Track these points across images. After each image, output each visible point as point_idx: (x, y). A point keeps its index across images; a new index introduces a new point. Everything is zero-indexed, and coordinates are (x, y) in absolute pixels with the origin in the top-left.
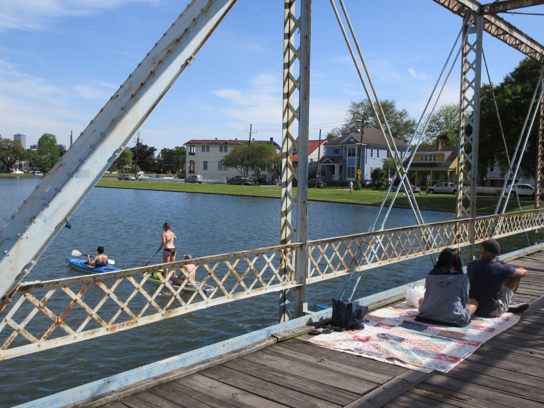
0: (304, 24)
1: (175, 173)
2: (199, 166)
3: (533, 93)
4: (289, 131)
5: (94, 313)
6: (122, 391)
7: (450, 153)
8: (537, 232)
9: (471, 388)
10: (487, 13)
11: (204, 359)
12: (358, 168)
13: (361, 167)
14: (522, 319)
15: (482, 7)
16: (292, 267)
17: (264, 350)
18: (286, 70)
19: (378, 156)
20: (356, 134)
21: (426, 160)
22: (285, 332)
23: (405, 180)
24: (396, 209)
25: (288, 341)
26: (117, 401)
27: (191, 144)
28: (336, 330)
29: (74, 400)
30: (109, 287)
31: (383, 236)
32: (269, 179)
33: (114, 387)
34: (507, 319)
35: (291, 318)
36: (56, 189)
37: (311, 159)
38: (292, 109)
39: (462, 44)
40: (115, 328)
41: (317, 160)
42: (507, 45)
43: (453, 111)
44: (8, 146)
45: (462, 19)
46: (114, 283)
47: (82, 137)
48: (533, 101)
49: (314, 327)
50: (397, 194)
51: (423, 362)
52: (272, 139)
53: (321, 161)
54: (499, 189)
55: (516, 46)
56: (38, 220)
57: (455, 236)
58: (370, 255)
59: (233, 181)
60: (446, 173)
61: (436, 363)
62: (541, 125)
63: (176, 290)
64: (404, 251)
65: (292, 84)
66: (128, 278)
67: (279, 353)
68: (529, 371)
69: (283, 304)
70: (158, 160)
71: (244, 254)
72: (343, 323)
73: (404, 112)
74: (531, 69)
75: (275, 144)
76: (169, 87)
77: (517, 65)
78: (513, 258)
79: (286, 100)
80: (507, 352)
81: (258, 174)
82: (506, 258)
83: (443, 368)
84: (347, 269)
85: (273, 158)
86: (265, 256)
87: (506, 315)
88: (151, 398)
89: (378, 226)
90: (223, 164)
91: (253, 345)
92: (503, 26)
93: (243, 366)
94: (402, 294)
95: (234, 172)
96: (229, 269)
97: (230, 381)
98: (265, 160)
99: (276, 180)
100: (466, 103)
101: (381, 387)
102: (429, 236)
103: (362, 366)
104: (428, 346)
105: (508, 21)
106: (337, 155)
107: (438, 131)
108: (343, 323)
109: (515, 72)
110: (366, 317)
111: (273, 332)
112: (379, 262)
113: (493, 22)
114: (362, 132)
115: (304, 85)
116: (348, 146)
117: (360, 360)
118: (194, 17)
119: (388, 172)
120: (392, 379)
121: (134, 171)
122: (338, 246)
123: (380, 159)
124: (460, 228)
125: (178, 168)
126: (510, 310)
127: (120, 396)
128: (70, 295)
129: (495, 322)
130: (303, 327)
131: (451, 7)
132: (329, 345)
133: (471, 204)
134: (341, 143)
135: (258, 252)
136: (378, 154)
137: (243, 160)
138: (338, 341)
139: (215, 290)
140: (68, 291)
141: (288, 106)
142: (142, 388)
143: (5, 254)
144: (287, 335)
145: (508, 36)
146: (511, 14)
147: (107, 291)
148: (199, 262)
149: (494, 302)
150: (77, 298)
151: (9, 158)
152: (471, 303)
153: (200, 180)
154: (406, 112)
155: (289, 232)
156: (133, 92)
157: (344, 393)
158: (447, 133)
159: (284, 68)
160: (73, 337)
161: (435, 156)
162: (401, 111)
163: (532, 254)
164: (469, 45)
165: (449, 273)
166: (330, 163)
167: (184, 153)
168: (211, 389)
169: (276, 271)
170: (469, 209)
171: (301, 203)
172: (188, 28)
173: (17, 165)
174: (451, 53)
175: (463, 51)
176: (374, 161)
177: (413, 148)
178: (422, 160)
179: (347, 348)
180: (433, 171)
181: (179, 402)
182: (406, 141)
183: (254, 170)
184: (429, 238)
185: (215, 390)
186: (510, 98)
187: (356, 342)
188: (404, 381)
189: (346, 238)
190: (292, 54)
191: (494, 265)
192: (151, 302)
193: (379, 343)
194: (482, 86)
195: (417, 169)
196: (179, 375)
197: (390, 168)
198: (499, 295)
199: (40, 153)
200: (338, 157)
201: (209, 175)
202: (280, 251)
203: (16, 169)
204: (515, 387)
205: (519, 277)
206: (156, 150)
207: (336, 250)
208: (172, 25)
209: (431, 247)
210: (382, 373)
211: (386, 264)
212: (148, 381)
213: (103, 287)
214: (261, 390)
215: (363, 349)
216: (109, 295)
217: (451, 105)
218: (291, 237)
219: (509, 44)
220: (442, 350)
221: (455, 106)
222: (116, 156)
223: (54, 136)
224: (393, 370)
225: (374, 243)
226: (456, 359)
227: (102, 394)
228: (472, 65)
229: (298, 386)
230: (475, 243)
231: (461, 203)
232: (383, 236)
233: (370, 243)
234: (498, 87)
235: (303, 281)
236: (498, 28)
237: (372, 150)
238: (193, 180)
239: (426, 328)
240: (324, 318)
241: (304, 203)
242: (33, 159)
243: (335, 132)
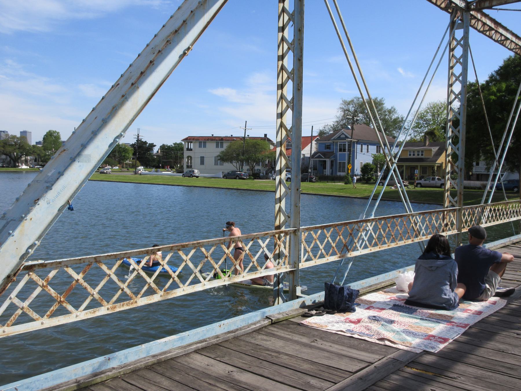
0: (297, 17)
1: (173, 168)
2: (196, 161)
5: (95, 292)
7: (437, 148)
9: (460, 368)
10: (473, 10)
11: (201, 339)
12: (349, 163)
13: (351, 162)
14: (508, 303)
16: (286, 252)
17: (259, 331)
18: (280, 63)
19: (368, 152)
20: (346, 131)
21: (414, 155)
22: (279, 314)
24: (383, 202)
26: (117, 377)
27: (189, 140)
28: (328, 313)
29: (75, 376)
30: (110, 268)
31: (374, 223)
32: (263, 173)
33: (114, 364)
34: (494, 303)
35: (285, 301)
36: (59, 173)
37: (304, 155)
38: (286, 100)
39: (450, 39)
40: (115, 307)
41: (309, 156)
42: (493, 41)
43: (440, 108)
44: (15, 142)
45: (449, 15)
46: (114, 264)
47: (84, 123)
49: (307, 310)
50: (385, 188)
51: (413, 342)
52: (266, 135)
53: (313, 156)
54: (485, 182)
55: (501, 42)
56: (41, 202)
57: (443, 225)
58: (361, 241)
59: (227, 176)
60: (433, 167)
61: (425, 344)
63: (174, 272)
64: (393, 238)
65: (285, 76)
67: (274, 334)
69: (277, 288)
72: (335, 306)
73: (392, 110)
74: (515, 67)
75: (269, 140)
76: (167, 76)
77: (501, 63)
78: (499, 246)
79: (280, 91)
81: (252, 169)
82: (490, 246)
83: (433, 348)
84: (339, 255)
86: (260, 241)
89: (369, 214)
90: (220, 159)
92: (489, 23)
93: (239, 346)
94: (392, 280)
95: (229, 167)
96: (225, 253)
97: (226, 359)
98: (259, 156)
99: (270, 174)
100: (453, 96)
102: (418, 225)
103: (354, 346)
104: (418, 327)
105: (493, 17)
106: (328, 150)
107: (425, 127)
108: (335, 306)
109: (499, 70)
110: (357, 301)
111: (267, 314)
112: (369, 249)
113: (479, 18)
114: (353, 128)
115: (297, 76)
116: (339, 142)
117: (352, 341)
118: (192, 9)
119: (377, 167)
120: (383, 358)
121: (134, 166)
122: (330, 232)
123: (369, 154)
124: (448, 217)
125: (176, 163)
126: (497, 295)
127: (120, 372)
129: (482, 306)
130: (297, 309)
131: (438, 3)
132: (322, 326)
133: (458, 194)
135: (253, 237)
137: (238, 155)
138: (331, 322)
139: (211, 275)
140: (71, 271)
141: (282, 97)
142: (141, 365)
143: (10, 234)
144: (281, 316)
145: (493, 32)
146: (496, 11)
147: (108, 272)
149: (481, 286)
150: (79, 278)
151: (15, 154)
152: (459, 287)
153: (197, 175)
154: (395, 110)
155: (283, 218)
157: (336, 371)
158: (434, 129)
159: (278, 60)
160: (75, 316)
161: (422, 152)
162: (390, 108)
163: (517, 243)
164: (456, 40)
165: (438, 258)
166: (322, 158)
167: (182, 149)
168: (208, 367)
170: (456, 199)
171: (295, 195)
173: (23, 161)
176: (364, 157)
177: (399, 145)
178: (410, 155)
179: (339, 330)
180: (421, 166)
181: (177, 378)
182: (394, 137)
183: (248, 165)
184: (418, 226)
185: (211, 368)
186: (495, 95)
187: (348, 324)
188: (395, 360)
189: (338, 225)
190: (286, 47)
193: (370, 325)
195: (405, 164)
196: (177, 354)
197: (379, 163)
198: (486, 280)
199: (45, 148)
202: (274, 236)
203: (22, 164)
204: (503, 367)
205: (506, 262)
206: (155, 146)
207: (328, 236)
208: (171, 17)
209: (420, 234)
210: (373, 352)
211: (376, 250)
212: (147, 359)
213: (104, 267)
214: (256, 368)
215: (355, 330)
216: (109, 275)
217: (438, 103)
218: (285, 222)
219: (494, 40)
220: (431, 331)
221: (441, 103)
223: (58, 133)
224: (384, 350)
225: (364, 230)
226: (445, 340)
227: (103, 371)
228: (459, 59)
230: (462, 232)
231: (449, 193)
232: (374, 223)
233: (361, 230)
234: (483, 85)
235: (296, 265)
236: (484, 24)
237: (362, 145)
238: (191, 175)
239: (415, 311)
240: (317, 301)
241: (298, 190)
242: (39, 155)
243: (327, 129)
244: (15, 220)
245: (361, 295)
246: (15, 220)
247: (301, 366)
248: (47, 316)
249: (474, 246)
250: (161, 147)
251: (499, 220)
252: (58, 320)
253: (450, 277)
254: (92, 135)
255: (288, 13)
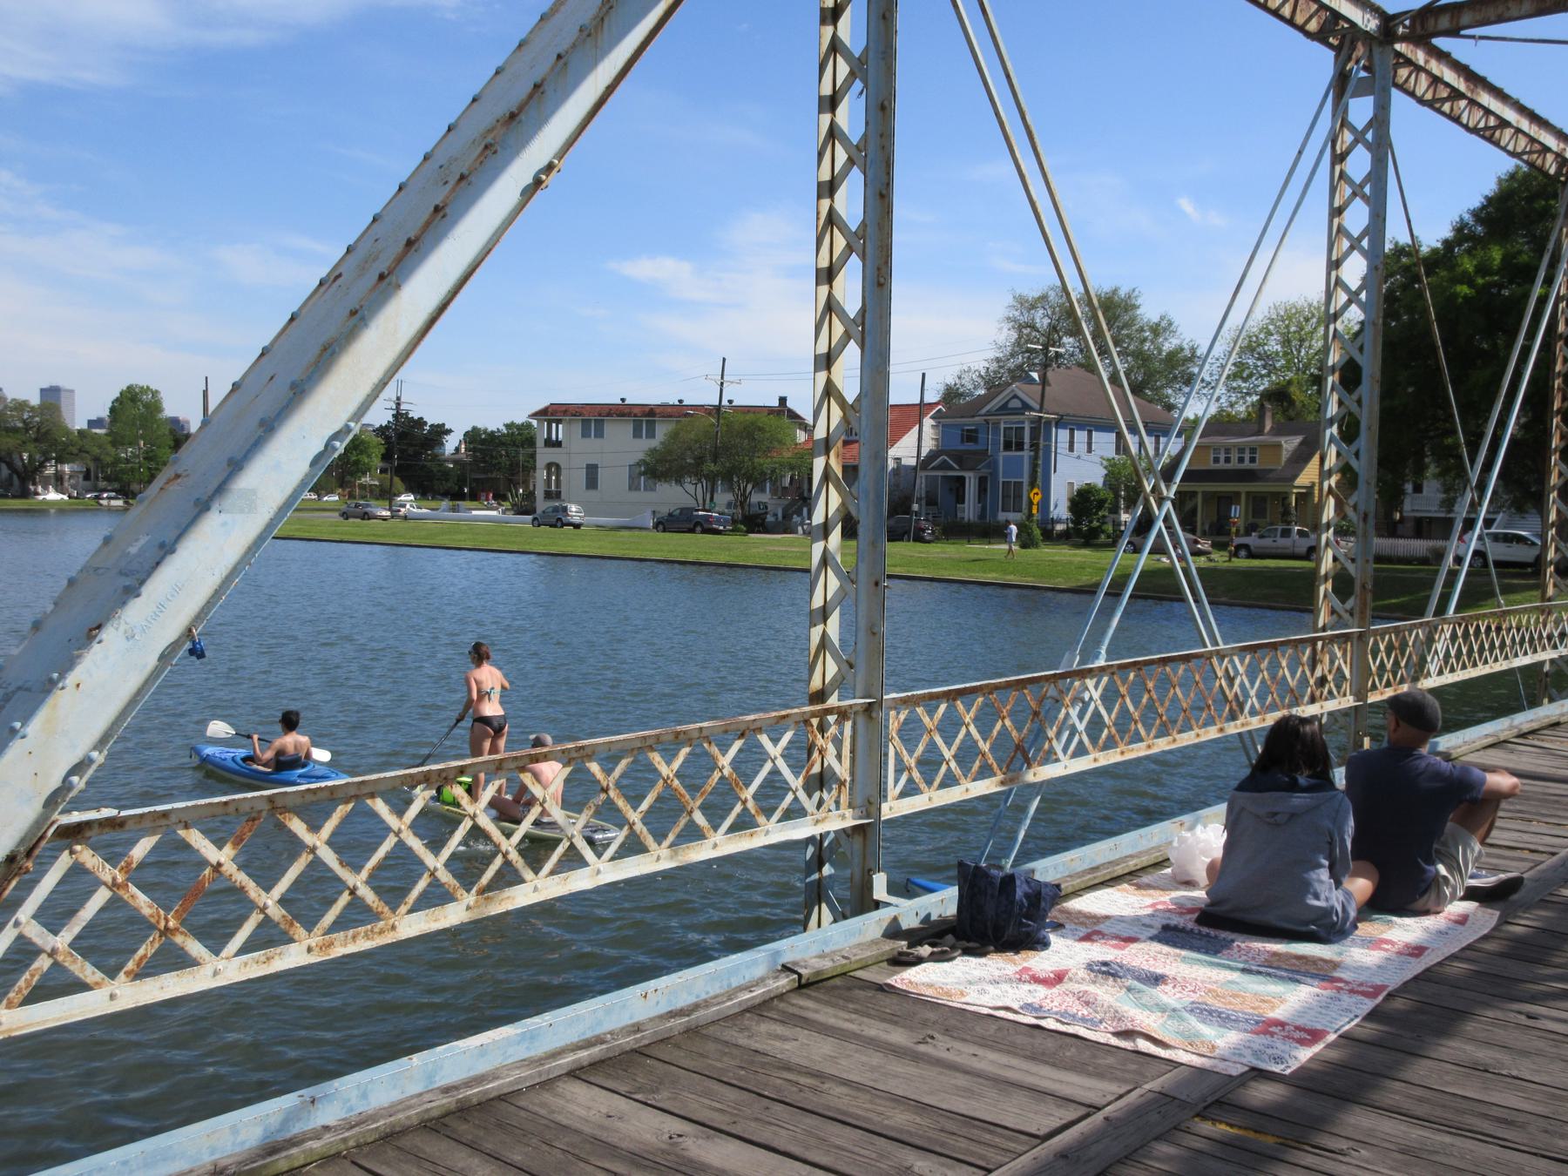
0: (877, 68)
1: (505, 498)
2: (574, 479)
3: (1537, 269)
4: (834, 378)
5: (270, 901)
6: (352, 1127)
7: (1297, 440)
8: (1547, 668)
9: (1359, 1120)
10: (1403, 39)
11: (589, 1035)
12: (1032, 485)
13: (1039, 481)
14: (1504, 921)
15: (1388, 21)
16: (842, 770)
17: (760, 1009)
18: (826, 203)
19: (1090, 450)
20: (1027, 387)
21: (1227, 460)
22: (822, 956)
23: (1167, 519)
24: (1140, 602)
25: (831, 982)
27: (551, 414)
28: (968, 952)
29: (212, 1154)
30: (314, 828)
31: (1105, 679)
32: (776, 515)
33: (328, 1115)
34: (1463, 920)
35: (839, 917)
36: (162, 545)
37: (898, 460)
38: (843, 315)
39: (1333, 127)
40: (331, 944)
41: (913, 462)
42: (1462, 130)
43: (1307, 320)
44: (24, 422)
45: (1332, 54)
48: (1537, 290)
49: (904, 943)
50: (1143, 560)
51: (1220, 1043)
52: (783, 400)
53: (924, 464)
54: (1439, 543)
55: (1488, 134)
56: (109, 634)
57: (1312, 682)
58: (1066, 734)
59: (671, 523)
60: (1284, 497)
61: (1256, 1047)
62: (1560, 361)
63: (508, 835)
64: (1164, 724)
65: (840, 243)
66: (369, 802)
67: (805, 1019)
68: (1524, 1069)
69: (816, 876)
70: (455, 462)
71: (705, 733)
72: (990, 933)
73: (1164, 324)
74: (1531, 199)
75: (793, 415)
76: (486, 251)
77: (1489, 187)
78: (1478, 745)
79: (824, 289)
80: (1462, 1014)
81: (743, 501)
82: (1459, 744)
83: (1278, 1059)
84: (1000, 777)
85: (787, 454)
86: (764, 739)
87: (1458, 907)
88: (434, 1147)
89: (1089, 653)
90: (644, 473)
91: (730, 995)
92: (1449, 76)
93: (702, 1055)
94: (1158, 848)
95: (674, 496)
96: (660, 775)
97: (662, 1098)
98: (764, 462)
99: (796, 518)
100: (1342, 297)
101: (1099, 1116)
102: (1237, 682)
103: (1043, 1054)
104: (1235, 996)
105: (1464, 61)
106: (970, 446)
107: (1262, 376)
108: (990, 933)
109: (1483, 207)
110: (1054, 914)
111: (787, 958)
112: (1091, 757)
113: (1421, 63)
114: (1044, 381)
115: (875, 244)
116: (1004, 422)
117: (1039, 1039)
118: (560, 50)
119: (1117, 496)
120: (1129, 1092)
121: (386, 494)
122: (974, 709)
123: (1094, 457)
124: (1327, 658)
125: (512, 483)
126: (1471, 894)
127: (345, 1140)
128: (203, 850)
129: (1426, 930)
130: (874, 942)
131: (1299, 20)
132: (948, 994)
133: (1357, 588)
134: (984, 411)
135: (743, 727)
136: (1090, 444)
137: (700, 460)
138: (975, 982)
139: (619, 836)
140: (196, 838)
141: (831, 307)
142: (408, 1118)
143: (14, 732)
144: (826, 964)
145: (1463, 103)
146: (1472, 41)
147: (308, 838)
148: (575, 755)
149: (1424, 871)
150: (222, 860)
151: (25, 456)
152: (1357, 874)
153: (576, 520)
154: (1170, 324)
155: (832, 669)
156: (382, 266)
157: (991, 1132)
158: (1290, 382)
159: (819, 197)
161: (1253, 450)
162: (1155, 319)
163: (1533, 732)
164: (1353, 129)
165: (1293, 787)
166: (952, 468)
167: (530, 442)
168: (607, 1122)
169: (796, 783)
170: (1350, 603)
171: (868, 586)
172: (543, 80)
173: (48, 477)
174: (1300, 152)
175: (1333, 147)
176: (1077, 465)
177: (1189, 428)
178: (1216, 460)
179: (1000, 1004)
180: (1248, 493)
181: (517, 1158)
182: (1170, 407)
183: (731, 489)
184: (1236, 687)
185: (620, 1124)
186: (1471, 284)
187: (1027, 987)
188: (1164, 1099)
189: (996, 687)
190: (841, 156)
191: (1423, 764)
192: (436, 869)
193: (1092, 988)
194: (1388, 247)
195: (1201, 487)
196: (517, 1081)
197: (1125, 483)
198: (1438, 852)
199: (116, 440)
200: (975, 453)
201: (603, 505)
202: (807, 722)
203: (45, 488)
204: (1485, 1116)
205: (1496, 798)
206: (449, 432)
207: (967, 720)
208: (497, 73)
209: (1242, 711)
210: (1100, 1075)
211: (1112, 761)
213: (297, 826)
214: (753, 1124)
215: (1047, 1005)
216: (313, 850)
217: (1301, 303)
218: (839, 682)
219: (1466, 127)
220: (1273, 1008)
221: (1310, 305)
222: (335, 449)
223: (155, 393)
224: (1134, 1067)
225: (1077, 699)
226: (1314, 1035)
228: (1362, 186)
229: (859, 1112)
230: (1370, 701)
231: (1329, 585)
232: (1105, 679)
233: (1067, 700)
234: (1434, 251)
235: (873, 809)
236: (1436, 80)
237: (1072, 431)
238: (558, 520)
239: (1227, 944)
240: (934, 917)
241: (877, 584)
242: (96, 459)
243: (967, 382)
244: (28, 690)
245: (1068, 896)
246: (28, 690)
247: (888, 1118)
248: (128, 974)
249: (1399, 754)
250: (466, 434)
251: (1480, 665)
252: (158, 984)
253: (1331, 843)
254: (260, 432)
255: (848, 56)
